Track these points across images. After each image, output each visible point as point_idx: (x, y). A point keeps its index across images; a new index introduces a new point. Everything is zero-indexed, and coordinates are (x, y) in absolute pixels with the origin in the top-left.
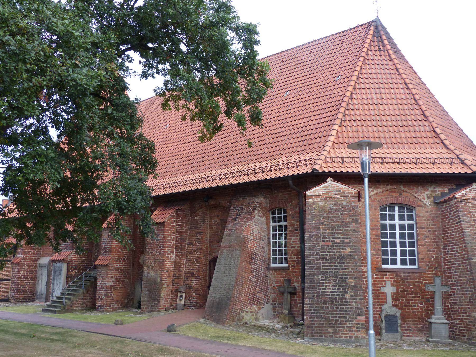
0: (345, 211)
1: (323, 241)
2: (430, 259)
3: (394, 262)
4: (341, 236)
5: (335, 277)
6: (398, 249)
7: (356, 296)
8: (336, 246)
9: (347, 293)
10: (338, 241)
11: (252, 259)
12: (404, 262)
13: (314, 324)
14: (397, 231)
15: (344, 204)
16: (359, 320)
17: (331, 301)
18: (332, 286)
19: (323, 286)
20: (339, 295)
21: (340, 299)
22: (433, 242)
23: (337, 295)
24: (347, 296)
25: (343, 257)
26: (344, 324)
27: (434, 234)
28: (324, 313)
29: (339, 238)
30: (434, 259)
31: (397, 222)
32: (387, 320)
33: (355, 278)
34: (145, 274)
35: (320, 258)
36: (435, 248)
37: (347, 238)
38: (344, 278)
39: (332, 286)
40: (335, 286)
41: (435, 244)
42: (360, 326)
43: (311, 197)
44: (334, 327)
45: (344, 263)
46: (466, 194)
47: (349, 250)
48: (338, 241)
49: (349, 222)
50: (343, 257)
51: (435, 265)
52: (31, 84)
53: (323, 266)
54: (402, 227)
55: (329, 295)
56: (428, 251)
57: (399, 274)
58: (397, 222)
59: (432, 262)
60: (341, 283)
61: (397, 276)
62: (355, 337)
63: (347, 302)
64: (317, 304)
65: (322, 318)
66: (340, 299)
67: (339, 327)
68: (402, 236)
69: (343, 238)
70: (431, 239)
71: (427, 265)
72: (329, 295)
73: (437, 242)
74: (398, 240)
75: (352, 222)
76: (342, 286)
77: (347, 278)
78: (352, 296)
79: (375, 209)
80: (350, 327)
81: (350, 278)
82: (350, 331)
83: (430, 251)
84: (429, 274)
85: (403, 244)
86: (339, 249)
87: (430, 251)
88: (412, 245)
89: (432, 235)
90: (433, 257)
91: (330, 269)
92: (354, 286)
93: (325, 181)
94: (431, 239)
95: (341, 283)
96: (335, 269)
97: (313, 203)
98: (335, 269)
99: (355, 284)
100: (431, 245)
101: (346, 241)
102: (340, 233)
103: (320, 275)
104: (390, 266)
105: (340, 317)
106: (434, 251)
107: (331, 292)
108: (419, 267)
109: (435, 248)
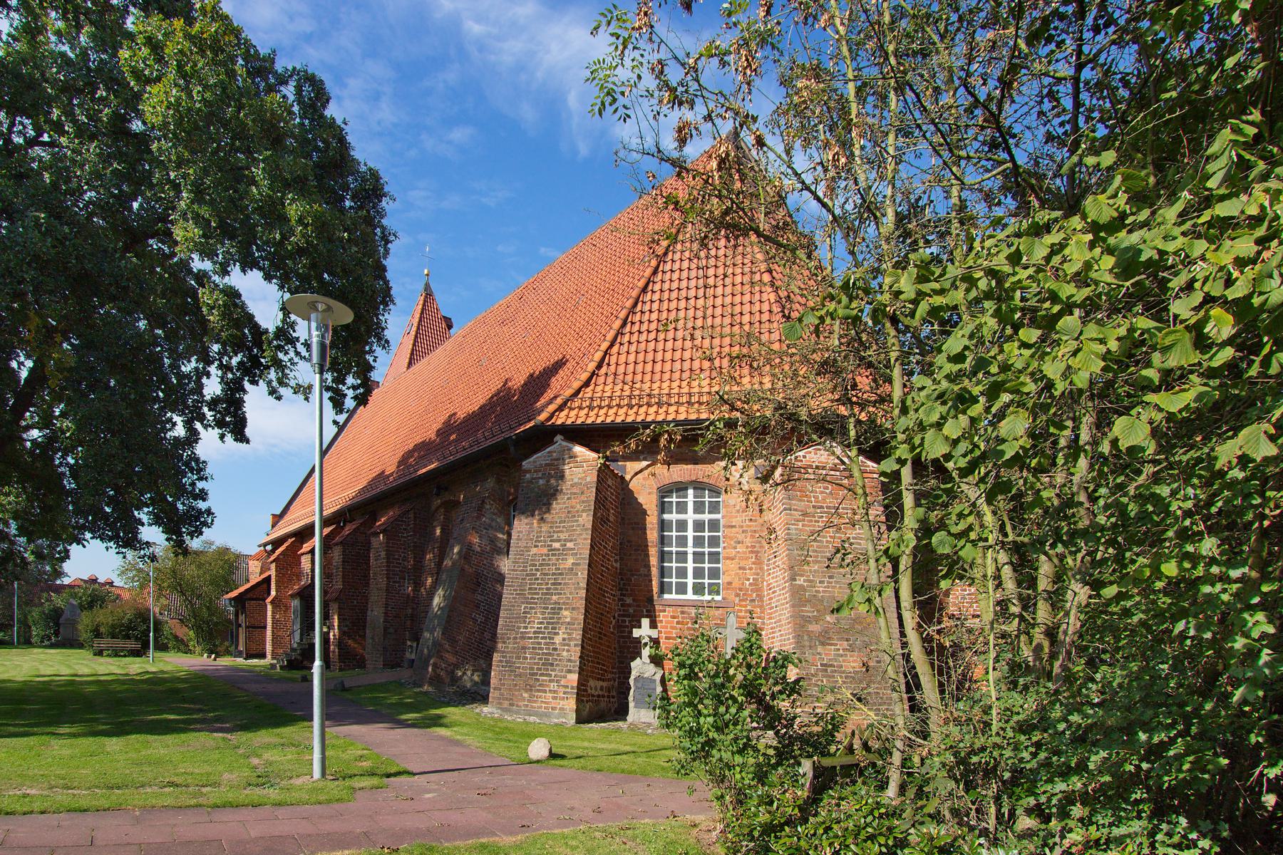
0: (575, 494)
1: (536, 546)
2: (743, 584)
3: (682, 589)
4: (562, 536)
5: (544, 608)
6: (690, 565)
7: (570, 639)
8: (553, 555)
9: (558, 634)
10: (556, 545)
11: (478, 584)
12: (698, 589)
13: (504, 684)
14: (690, 534)
15: (576, 480)
16: (569, 681)
17: (533, 648)
18: (538, 623)
19: (525, 622)
20: (545, 638)
21: (546, 644)
22: (752, 552)
23: (542, 638)
24: (558, 639)
25: (560, 574)
26: (547, 686)
27: (752, 536)
28: (519, 668)
29: (559, 541)
30: (750, 584)
31: (690, 516)
32: (639, 685)
33: (573, 609)
34: (369, 613)
35: (527, 575)
36: (754, 563)
37: (571, 541)
38: (557, 610)
39: (538, 623)
40: (541, 623)
41: (754, 555)
42: (569, 690)
43: (529, 471)
44: (531, 690)
45: (560, 584)
46: (804, 457)
47: (571, 561)
48: (556, 545)
49: (578, 511)
50: (560, 574)
51: (751, 595)
52: (1159, 585)
53: (530, 589)
54: (699, 526)
55: (531, 638)
56: (740, 568)
57: (686, 609)
58: (690, 516)
59: (747, 590)
60: (550, 618)
61: (683, 612)
62: (560, 709)
63: (555, 649)
64: (512, 652)
65: (516, 676)
66: (546, 644)
67: (539, 691)
68: (698, 541)
69: (565, 540)
70: (747, 547)
71: (738, 595)
72: (531, 638)
73: (758, 552)
74: (690, 549)
75: (583, 511)
76: (553, 623)
77: (561, 609)
78: (564, 639)
79: (650, 493)
80: (555, 692)
81: (566, 609)
82: (555, 698)
83: (744, 569)
84: (741, 611)
85: (698, 557)
86: (558, 560)
87: (744, 569)
88: (715, 557)
89: (748, 539)
90: (748, 580)
91: (538, 594)
92: (569, 623)
93: (552, 443)
94: (747, 547)
95: (550, 618)
96: (547, 594)
97: (530, 482)
98: (547, 594)
99: (572, 618)
100: (747, 558)
101: (570, 545)
102: (562, 532)
103: (523, 603)
104: (674, 596)
105: (542, 675)
106: (751, 569)
107: (535, 633)
108: (723, 599)
109: (754, 563)
